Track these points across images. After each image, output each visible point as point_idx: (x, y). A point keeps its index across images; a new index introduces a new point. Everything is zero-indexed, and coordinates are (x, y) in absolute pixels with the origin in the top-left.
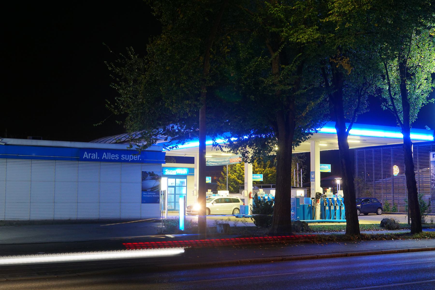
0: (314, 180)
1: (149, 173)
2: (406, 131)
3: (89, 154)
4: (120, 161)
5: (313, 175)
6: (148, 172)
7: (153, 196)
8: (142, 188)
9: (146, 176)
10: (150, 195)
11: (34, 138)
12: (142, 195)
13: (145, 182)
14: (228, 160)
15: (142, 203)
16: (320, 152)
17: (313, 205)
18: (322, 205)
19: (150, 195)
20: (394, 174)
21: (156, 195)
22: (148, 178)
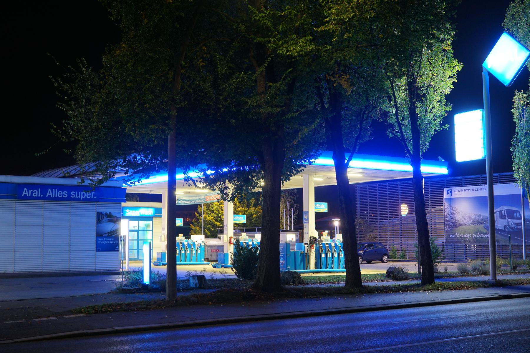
0: (307, 221)
1: (106, 214)
3: (30, 191)
4: (69, 199)
6: (104, 213)
7: (111, 242)
12: (97, 241)
13: (100, 225)
14: (204, 197)
15: (97, 251)
18: (317, 251)
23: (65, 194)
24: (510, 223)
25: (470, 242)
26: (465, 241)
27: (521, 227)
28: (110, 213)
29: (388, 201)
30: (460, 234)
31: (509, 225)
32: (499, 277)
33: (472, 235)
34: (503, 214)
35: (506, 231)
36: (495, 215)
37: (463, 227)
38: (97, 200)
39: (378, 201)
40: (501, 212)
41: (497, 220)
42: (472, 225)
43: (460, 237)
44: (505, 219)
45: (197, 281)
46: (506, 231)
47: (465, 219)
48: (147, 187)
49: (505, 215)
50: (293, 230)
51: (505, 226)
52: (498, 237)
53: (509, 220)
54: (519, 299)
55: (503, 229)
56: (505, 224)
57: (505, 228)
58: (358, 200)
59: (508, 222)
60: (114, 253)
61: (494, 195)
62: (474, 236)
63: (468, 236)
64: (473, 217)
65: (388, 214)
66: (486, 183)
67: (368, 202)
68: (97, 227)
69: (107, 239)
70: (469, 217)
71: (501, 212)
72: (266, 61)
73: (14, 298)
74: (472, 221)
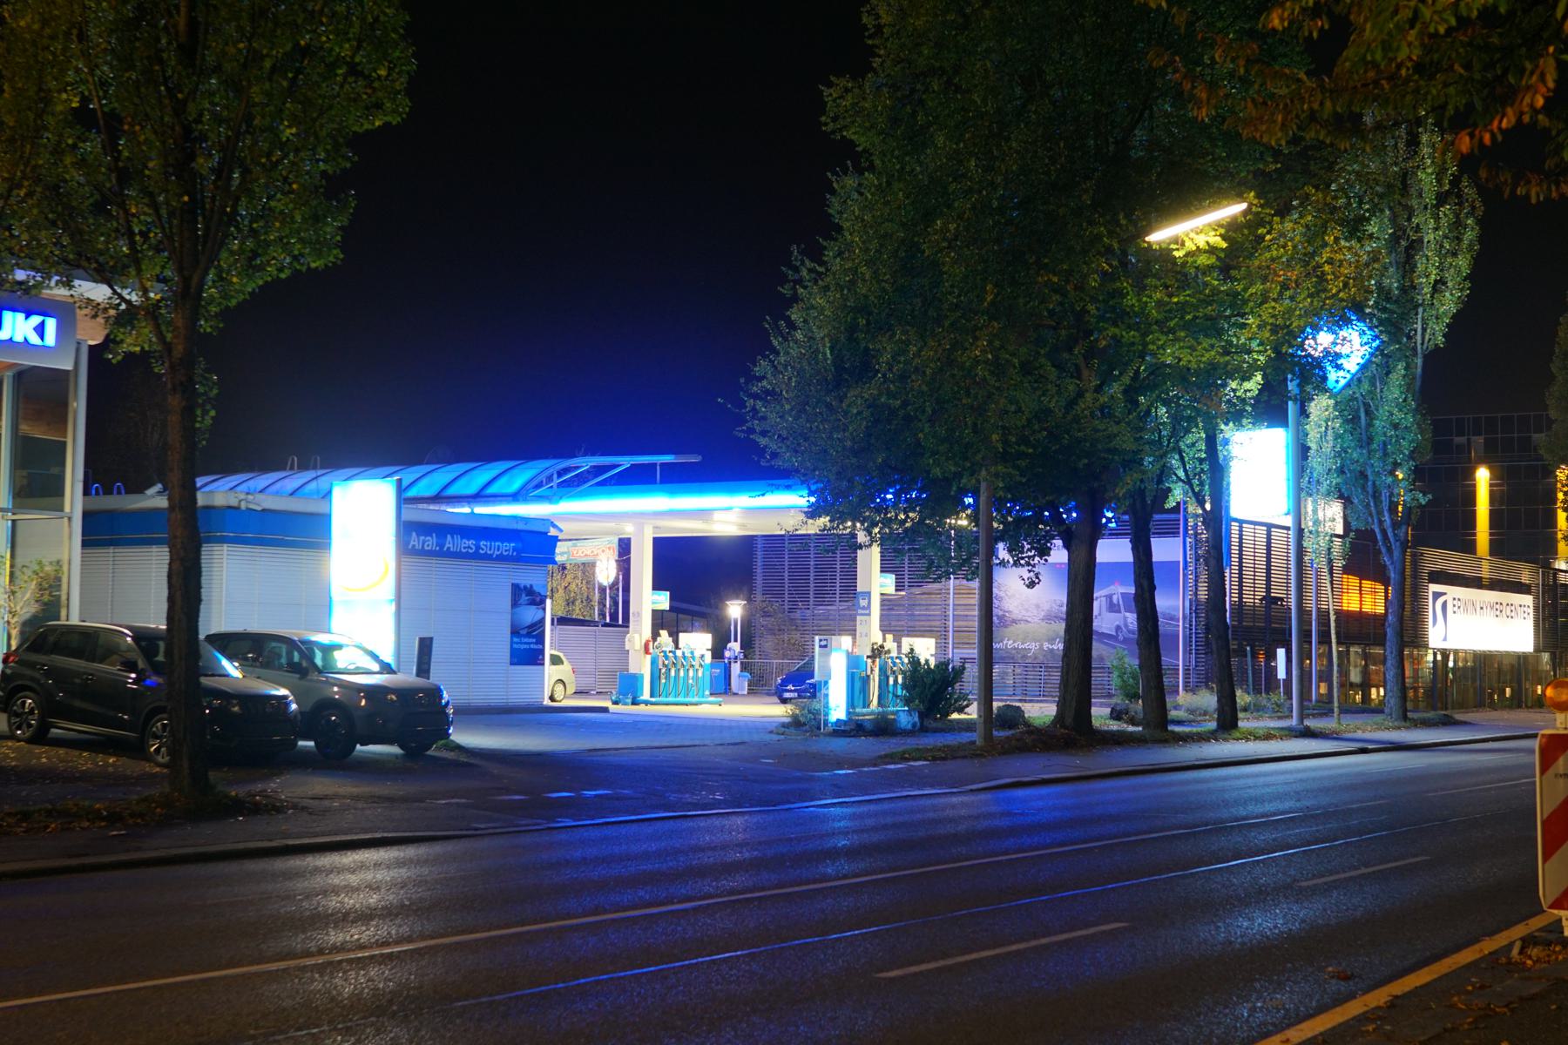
0: (867, 612)
1: (525, 587)
2: (472, 513)
3: (422, 538)
4: (477, 556)
5: (866, 601)
6: (522, 586)
7: (532, 646)
8: (513, 626)
9: (520, 596)
10: (526, 643)
11: (602, 455)
12: (512, 643)
13: (518, 610)
14: (566, 550)
15: (511, 664)
16: (655, 539)
17: (869, 673)
18: (883, 671)
19: (526, 643)
20: (167, 549)
21: (536, 643)
22: (521, 601)
23: (468, 544)
24: (1129, 620)
25: (1036, 658)
26: (1024, 657)
27: (956, 624)
28: (531, 586)
29: (838, 563)
30: (1014, 642)
31: (1126, 626)
32: (1307, 722)
33: (1041, 645)
34: (1115, 601)
35: (1121, 638)
36: (1096, 604)
37: (1022, 626)
38: (516, 559)
39: (812, 563)
40: (1110, 597)
41: (1100, 614)
42: (1043, 624)
43: (1014, 648)
44: (1119, 612)
45: (916, 719)
46: (1121, 638)
47: (1027, 610)
48: (1311, 580)
49: (1119, 605)
50: (620, 622)
51: (1118, 628)
52: (1098, 649)
53: (1128, 614)
54: (1490, 754)
55: (1114, 633)
56: (1117, 623)
57: (1117, 632)
58: (759, 557)
59: (1125, 618)
60: (540, 667)
61: (1154, 560)
62: (1046, 646)
63: (1033, 647)
64: (1046, 607)
65: (838, 589)
66: (1179, 533)
67: (786, 563)
68: (512, 614)
69: (526, 640)
70: (1038, 606)
71: (1110, 597)
72: (404, 116)
73: (645, 744)
74: (1043, 614)
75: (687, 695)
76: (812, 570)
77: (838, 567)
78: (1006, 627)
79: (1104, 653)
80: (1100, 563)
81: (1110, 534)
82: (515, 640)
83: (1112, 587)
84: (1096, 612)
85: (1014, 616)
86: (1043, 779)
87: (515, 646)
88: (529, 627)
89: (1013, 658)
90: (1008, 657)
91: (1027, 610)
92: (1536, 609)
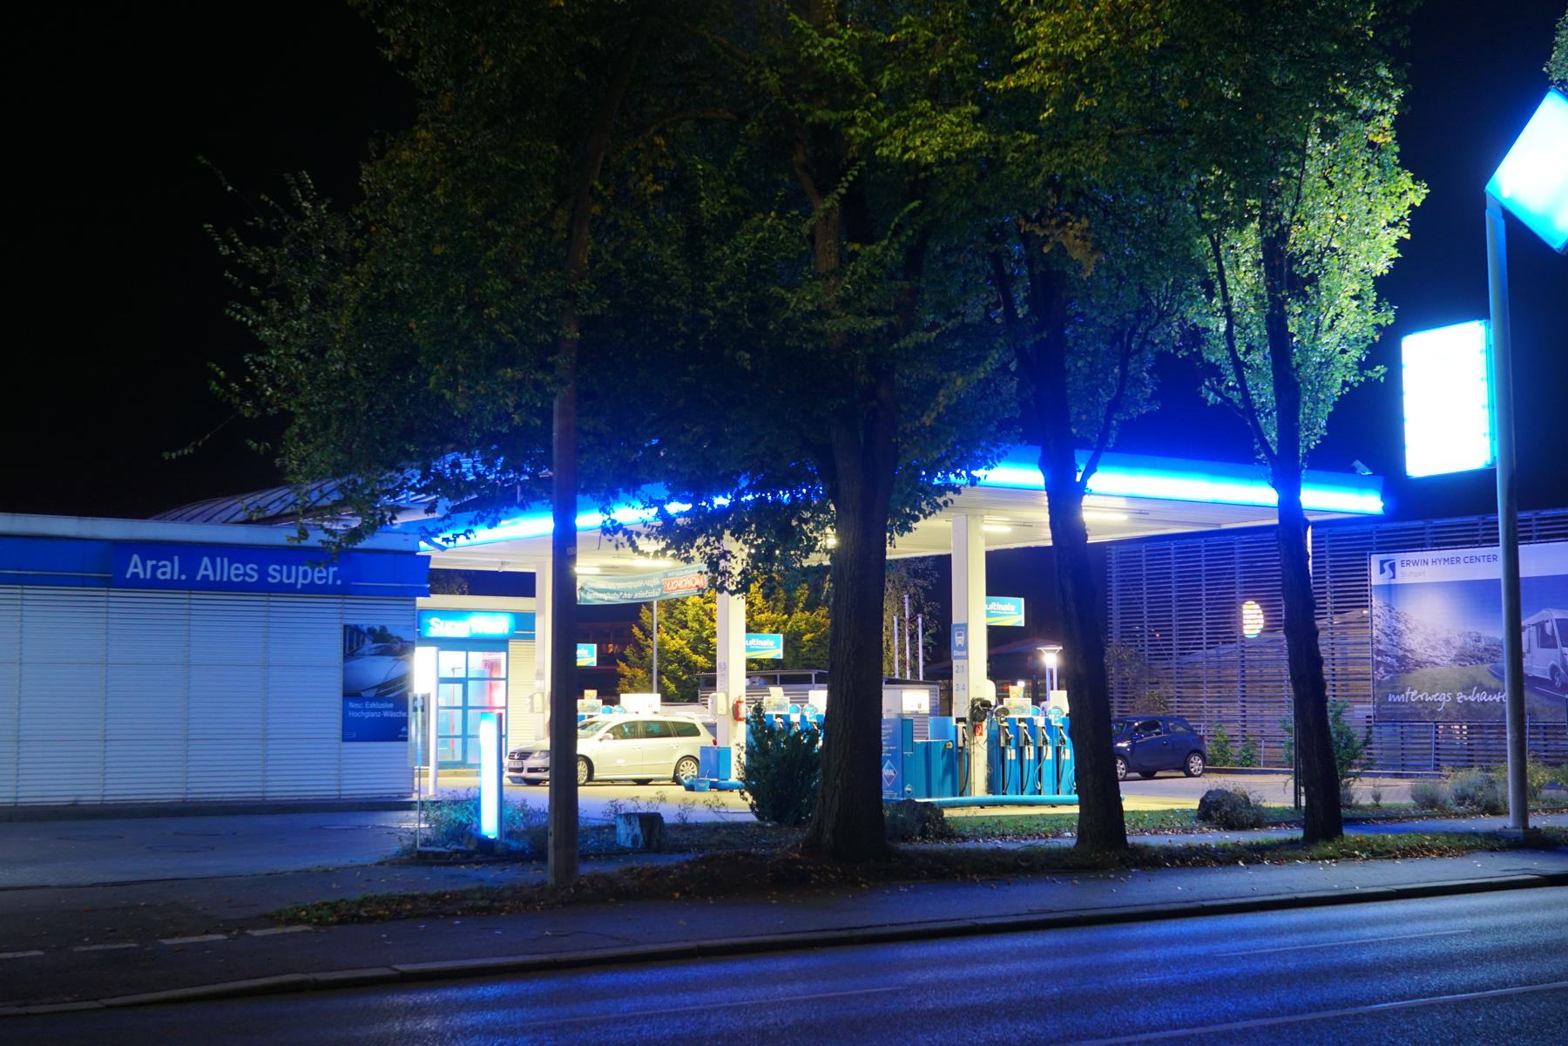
0: (964, 653)
1: (371, 631)
3: (150, 563)
4: (263, 587)
6: (365, 628)
7: (386, 714)
9: (360, 643)
14: (658, 583)
15: (345, 739)
18: (993, 742)
21: (394, 710)
25: (1447, 715)
26: (1433, 712)
30: (1419, 693)
32: (1535, 821)
33: (1454, 696)
34: (1548, 631)
35: (1558, 684)
37: (1428, 670)
39: (1173, 594)
40: (1541, 626)
41: (1529, 651)
42: (1456, 667)
43: (1419, 701)
44: (1555, 646)
45: (638, 830)
46: (1558, 684)
47: (1434, 648)
49: (1553, 637)
51: (1554, 669)
55: (1548, 677)
56: (1552, 662)
57: (1552, 676)
58: (1114, 589)
61: (1522, 575)
62: (1460, 697)
63: (1444, 698)
64: (1458, 642)
68: (345, 670)
69: (373, 705)
70: (1447, 642)
71: (1541, 626)
74: (1454, 652)
75: (1225, 763)
76: (1174, 604)
77: (1204, 598)
78: (1408, 672)
79: (1536, 705)
80: (1528, 579)
81: (1539, 537)
82: (352, 705)
83: (1544, 612)
84: (1525, 648)
85: (1417, 657)
86: (403, 974)
87: (352, 714)
88: (380, 687)
89: (1418, 715)
90: (1412, 714)
91: (1434, 648)
92: (1242, 625)
